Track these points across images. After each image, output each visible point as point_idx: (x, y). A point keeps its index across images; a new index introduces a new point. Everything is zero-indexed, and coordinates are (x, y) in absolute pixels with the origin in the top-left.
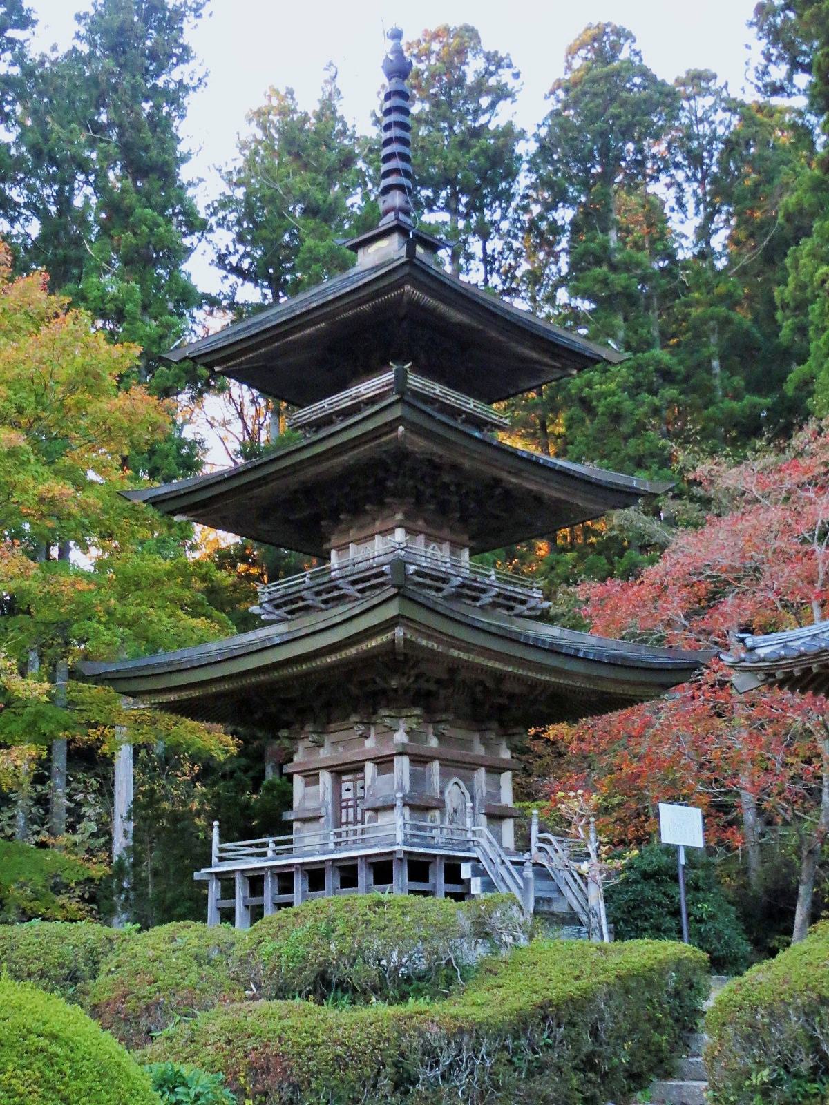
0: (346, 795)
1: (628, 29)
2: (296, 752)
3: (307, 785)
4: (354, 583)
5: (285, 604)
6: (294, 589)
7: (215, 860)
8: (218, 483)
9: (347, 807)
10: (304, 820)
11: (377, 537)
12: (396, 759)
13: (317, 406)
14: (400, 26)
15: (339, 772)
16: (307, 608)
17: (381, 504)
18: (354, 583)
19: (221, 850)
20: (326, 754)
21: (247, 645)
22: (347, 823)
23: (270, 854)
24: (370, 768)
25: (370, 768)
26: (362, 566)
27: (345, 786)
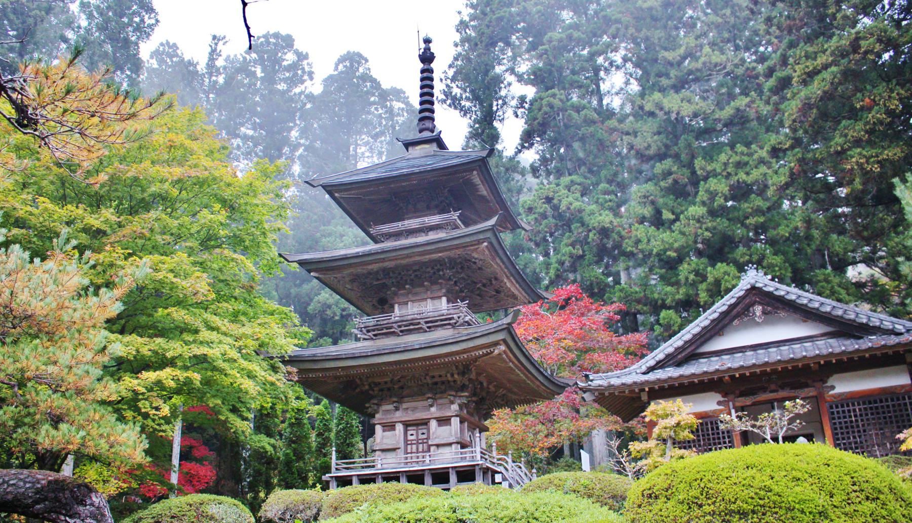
0: (410, 438)
1: (399, 88)
2: (378, 412)
3: (384, 431)
4: (427, 322)
5: (374, 330)
6: (385, 322)
7: (333, 469)
8: (433, 243)
9: (411, 444)
10: (383, 450)
11: (429, 301)
12: (453, 419)
13: (395, 224)
14: (430, 36)
15: (407, 425)
16: (393, 333)
17: (434, 283)
18: (427, 322)
19: (337, 464)
20: (399, 415)
21: (314, 355)
22: (411, 453)
23: (428, 462)
24: (433, 424)
25: (433, 424)
26: (410, 317)
27: (410, 433)
